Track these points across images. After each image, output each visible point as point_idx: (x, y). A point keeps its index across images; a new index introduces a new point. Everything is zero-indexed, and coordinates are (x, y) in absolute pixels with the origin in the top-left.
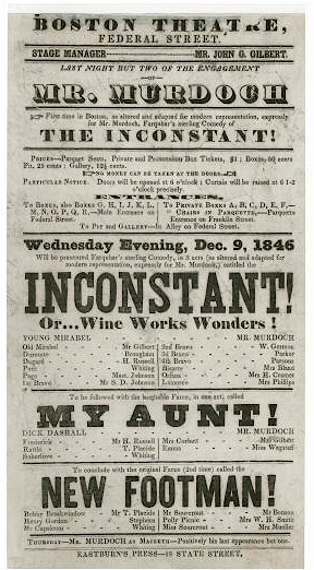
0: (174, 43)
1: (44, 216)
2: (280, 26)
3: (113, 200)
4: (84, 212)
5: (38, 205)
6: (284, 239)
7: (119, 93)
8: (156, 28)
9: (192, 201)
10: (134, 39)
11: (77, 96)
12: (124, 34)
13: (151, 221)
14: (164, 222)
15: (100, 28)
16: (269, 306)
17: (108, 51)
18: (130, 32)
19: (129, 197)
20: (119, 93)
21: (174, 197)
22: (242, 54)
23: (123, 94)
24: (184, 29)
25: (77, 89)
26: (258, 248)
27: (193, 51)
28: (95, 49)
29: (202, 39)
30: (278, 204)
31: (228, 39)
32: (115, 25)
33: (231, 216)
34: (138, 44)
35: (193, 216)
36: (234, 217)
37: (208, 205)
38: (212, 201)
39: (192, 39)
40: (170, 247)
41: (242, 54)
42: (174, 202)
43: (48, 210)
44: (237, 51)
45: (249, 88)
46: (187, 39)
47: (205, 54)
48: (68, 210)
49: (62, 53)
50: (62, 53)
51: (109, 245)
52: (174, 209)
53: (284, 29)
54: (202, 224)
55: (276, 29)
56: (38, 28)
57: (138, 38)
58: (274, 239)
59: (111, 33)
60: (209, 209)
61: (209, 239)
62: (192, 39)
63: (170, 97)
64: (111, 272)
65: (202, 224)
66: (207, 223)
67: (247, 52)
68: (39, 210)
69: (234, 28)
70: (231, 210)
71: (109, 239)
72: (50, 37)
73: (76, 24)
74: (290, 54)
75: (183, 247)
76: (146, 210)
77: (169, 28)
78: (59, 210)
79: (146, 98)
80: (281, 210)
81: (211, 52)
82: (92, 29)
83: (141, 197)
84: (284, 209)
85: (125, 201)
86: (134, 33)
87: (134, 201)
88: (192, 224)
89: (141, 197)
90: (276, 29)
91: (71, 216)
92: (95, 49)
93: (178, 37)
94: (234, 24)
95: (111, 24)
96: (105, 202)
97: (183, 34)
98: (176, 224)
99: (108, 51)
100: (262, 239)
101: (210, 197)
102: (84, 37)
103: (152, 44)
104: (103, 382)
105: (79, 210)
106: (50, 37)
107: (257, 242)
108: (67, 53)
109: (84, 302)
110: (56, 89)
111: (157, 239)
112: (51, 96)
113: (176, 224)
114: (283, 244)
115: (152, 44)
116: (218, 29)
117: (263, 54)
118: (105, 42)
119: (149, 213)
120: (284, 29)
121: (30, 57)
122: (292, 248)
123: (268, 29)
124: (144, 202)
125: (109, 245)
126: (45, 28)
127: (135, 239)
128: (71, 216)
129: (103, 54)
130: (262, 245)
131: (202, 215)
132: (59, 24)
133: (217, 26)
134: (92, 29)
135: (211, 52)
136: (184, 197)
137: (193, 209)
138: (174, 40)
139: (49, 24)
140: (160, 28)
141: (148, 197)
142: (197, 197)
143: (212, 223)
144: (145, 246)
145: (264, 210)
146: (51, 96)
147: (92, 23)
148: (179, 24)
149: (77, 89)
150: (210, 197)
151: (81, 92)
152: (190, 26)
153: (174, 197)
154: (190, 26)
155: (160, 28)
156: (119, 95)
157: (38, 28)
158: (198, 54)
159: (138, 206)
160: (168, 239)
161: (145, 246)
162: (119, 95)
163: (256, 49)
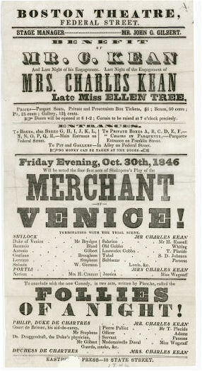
0: (109, 25)
1: (26, 139)
2: (176, 14)
3: (70, 128)
4: (51, 136)
5: (22, 131)
6: (173, 158)
7: (29, 58)
8: (96, 16)
9: (122, 129)
10: (83, 23)
11: (53, 60)
12: (77, 20)
13: (95, 141)
14: (103, 140)
15: (61, 15)
16: (105, 221)
17: (65, 30)
18: (80, 18)
19: (81, 126)
20: (29, 58)
21: (110, 126)
22: (151, 33)
23: (31, 59)
24: (114, 16)
25: (54, 55)
26: (156, 164)
27: (120, 30)
28: (57, 29)
29: (127, 22)
30: (156, 131)
31: (142, 21)
32: (71, 14)
33: (146, 139)
34: (86, 26)
35: (122, 139)
36: (148, 140)
37: (131, 131)
38: (134, 129)
39: (121, 23)
40: (88, 163)
41: (151, 33)
42: (108, 129)
43: (28, 135)
44: (148, 30)
45: (84, 55)
46: (118, 22)
47: (128, 33)
48: (41, 135)
49: (36, 32)
50: (36, 32)
51: (51, 162)
52: (109, 134)
53: (179, 16)
54: (127, 143)
55: (173, 16)
56: (20, 16)
57: (86, 22)
58: (166, 159)
59: (68, 19)
60: (131, 134)
61: (111, 158)
62: (121, 23)
63: (48, 60)
64: (79, 176)
65: (127, 143)
66: (131, 143)
67: (155, 31)
68: (22, 135)
69: (147, 16)
70: (146, 134)
71: (50, 158)
72: (28, 21)
73: (45, 14)
74: (183, 32)
75: (97, 164)
76: (91, 134)
77: (104, 15)
78: (35, 135)
79: (82, 60)
80: (178, 134)
81: (132, 31)
82: (56, 16)
83: (88, 126)
84: (179, 134)
85: (77, 129)
86: (83, 19)
87: (83, 129)
88: (121, 143)
89: (88, 126)
90: (173, 16)
91: (43, 138)
92: (57, 29)
93: (112, 21)
94: (147, 13)
95: (68, 13)
96: (65, 130)
97: (115, 19)
98: (111, 143)
99: (65, 30)
100: (159, 158)
101: (133, 126)
102: (51, 21)
103: (95, 26)
104: (70, 274)
105: (48, 135)
106: (28, 21)
107: (155, 160)
108: (39, 32)
109: (91, 194)
110: (37, 55)
111: (80, 158)
112: (34, 60)
113: (111, 143)
114: (172, 161)
115: (95, 26)
116: (137, 16)
117: (165, 32)
118: (65, 25)
119: (93, 136)
120: (179, 16)
121: (181, 30)
122: (178, 163)
123: (168, 16)
124: (90, 129)
125: (51, 162)
126: (25, 16)
127: (66, 158)
128: (43, 138)
129: (63, 32)
130: (158, 162)
131: (127, 138)
132: (34, 14)
133: (136, 15)
134: (56, 16)
135: (132, 31)
136: (116, 126)
137: (121, 134)
138: (109, 23)
139: (27, 13)
140: (99, 16)
141: (93, 126)
142: (125, 126)
143: (134, 143)
144: (73, 163)
145: (167, 134)
146: (34, 60)
147: (56, 13)
148: (112, 13)
149: (54, 55)
150: (133, 126)
151: (56, 57)
152: (118, 14)
153: (110, 126)
154: (118, 14)
155: (99, 16)
156: (29, 59)
157: (20, 16)
158: (124, 32)
159: (86, 132)
160: (87, 158)
161: (73, 163)
162: (29, 59)
163: (160, 29)
